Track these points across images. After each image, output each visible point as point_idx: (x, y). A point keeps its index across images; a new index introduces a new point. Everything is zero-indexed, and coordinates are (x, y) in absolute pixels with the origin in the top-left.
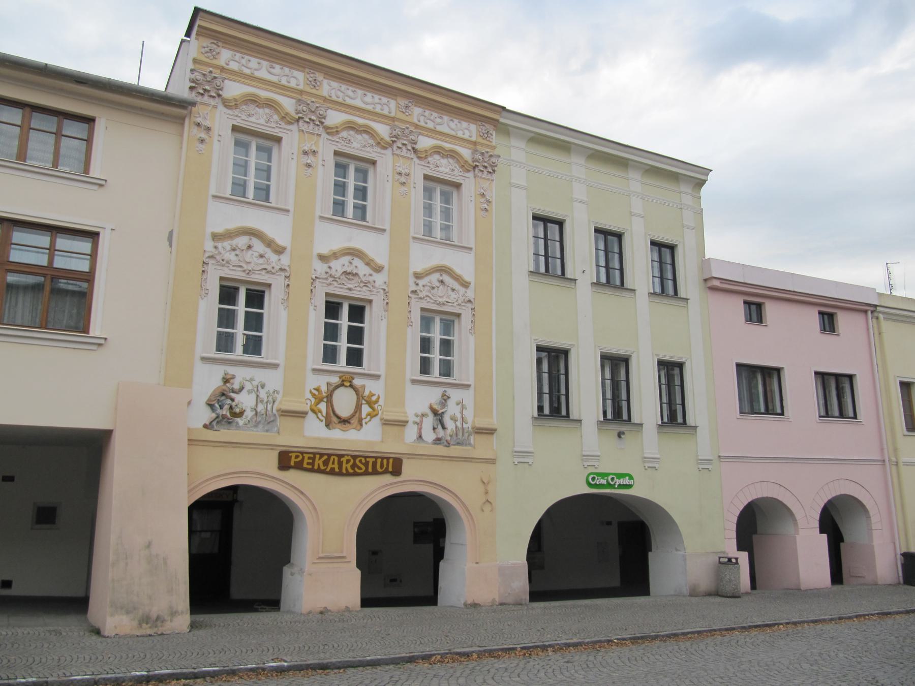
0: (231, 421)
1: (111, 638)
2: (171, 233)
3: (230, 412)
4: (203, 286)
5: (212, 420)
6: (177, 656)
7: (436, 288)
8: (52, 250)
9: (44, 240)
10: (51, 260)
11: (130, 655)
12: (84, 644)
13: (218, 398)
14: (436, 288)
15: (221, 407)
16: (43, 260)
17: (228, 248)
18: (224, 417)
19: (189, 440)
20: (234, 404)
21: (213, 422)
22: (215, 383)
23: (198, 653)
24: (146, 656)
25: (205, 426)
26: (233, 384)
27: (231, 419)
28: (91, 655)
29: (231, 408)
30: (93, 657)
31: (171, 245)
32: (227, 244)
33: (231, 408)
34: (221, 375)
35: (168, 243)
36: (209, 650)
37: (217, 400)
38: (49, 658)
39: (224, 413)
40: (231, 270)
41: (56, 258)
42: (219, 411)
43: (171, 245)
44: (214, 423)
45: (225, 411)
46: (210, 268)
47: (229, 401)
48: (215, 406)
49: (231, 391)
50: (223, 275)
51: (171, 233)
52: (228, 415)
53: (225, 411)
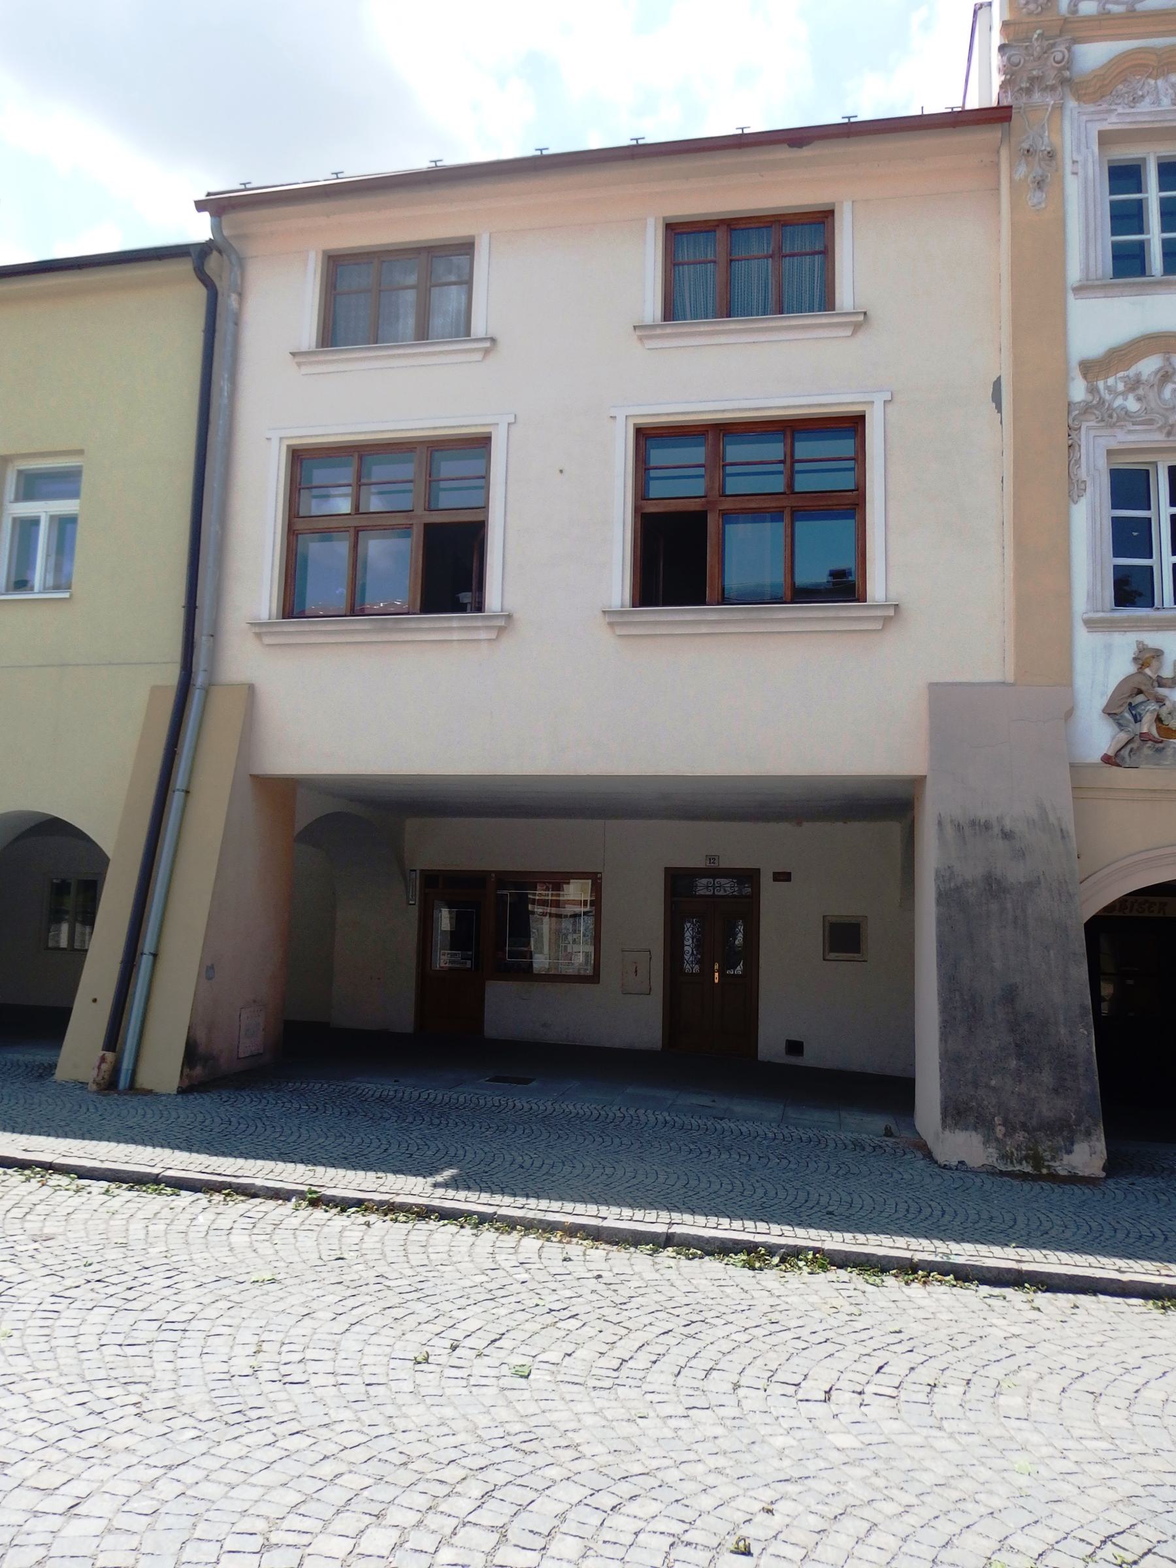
0: (1161, 745)
1: (951, 1169)
2: (997, 384)
3: (1158, 728)
4: (1072, 477)
5: (1119, 746)
6: (1083, 1232)
7: (612, 1451)
8: (790, 460)
9: (774, 450)
10: (791, 483)
11: (985, 1215)
12: (900, 1176)
13: (1129, 701)
14: (612, 1451)
15: (1137, 719)
16: (777, 484)
17: (1121, 387)
18: (1144, 738)
19: (1074, 788)
20: (1164, 712)
21: (1122, 752)
22: (1122, 667)
23: (1129, 1233)
24: (1015, 1221)
25: (1107, 760)
26: (1159, 668)
27: (1161, 742)
28: (910, 1201)
29: (1159, 719)
30: (914, 1208)
31: (999, 408)
32: (1115, 381)
33: (1159, 719)
34: (1131, 652)
35: (994, 405)
36: (1153, 1229)
37: (1126, 705)
38: (835, 1197)
39: (1145, 730)
40: (1130, 432)
41: (798, 477)
42: (1133, 726)
43: (999, 408)
44: (1125, 752)
45: (1147, 726)
46: (1085, 438)
47: (1153, 706)
48: (1123, 717)
49: (1156, 684)
50: (1114, 445)
51: (997, 384)
52: (1154, 732)
53: (1147, 726)
